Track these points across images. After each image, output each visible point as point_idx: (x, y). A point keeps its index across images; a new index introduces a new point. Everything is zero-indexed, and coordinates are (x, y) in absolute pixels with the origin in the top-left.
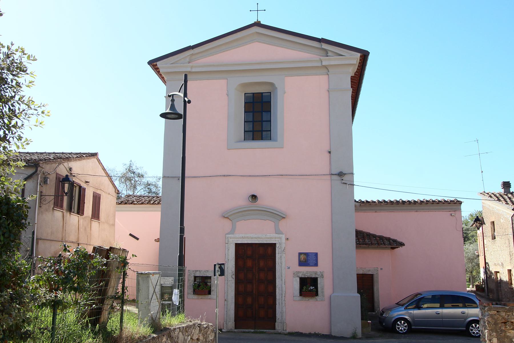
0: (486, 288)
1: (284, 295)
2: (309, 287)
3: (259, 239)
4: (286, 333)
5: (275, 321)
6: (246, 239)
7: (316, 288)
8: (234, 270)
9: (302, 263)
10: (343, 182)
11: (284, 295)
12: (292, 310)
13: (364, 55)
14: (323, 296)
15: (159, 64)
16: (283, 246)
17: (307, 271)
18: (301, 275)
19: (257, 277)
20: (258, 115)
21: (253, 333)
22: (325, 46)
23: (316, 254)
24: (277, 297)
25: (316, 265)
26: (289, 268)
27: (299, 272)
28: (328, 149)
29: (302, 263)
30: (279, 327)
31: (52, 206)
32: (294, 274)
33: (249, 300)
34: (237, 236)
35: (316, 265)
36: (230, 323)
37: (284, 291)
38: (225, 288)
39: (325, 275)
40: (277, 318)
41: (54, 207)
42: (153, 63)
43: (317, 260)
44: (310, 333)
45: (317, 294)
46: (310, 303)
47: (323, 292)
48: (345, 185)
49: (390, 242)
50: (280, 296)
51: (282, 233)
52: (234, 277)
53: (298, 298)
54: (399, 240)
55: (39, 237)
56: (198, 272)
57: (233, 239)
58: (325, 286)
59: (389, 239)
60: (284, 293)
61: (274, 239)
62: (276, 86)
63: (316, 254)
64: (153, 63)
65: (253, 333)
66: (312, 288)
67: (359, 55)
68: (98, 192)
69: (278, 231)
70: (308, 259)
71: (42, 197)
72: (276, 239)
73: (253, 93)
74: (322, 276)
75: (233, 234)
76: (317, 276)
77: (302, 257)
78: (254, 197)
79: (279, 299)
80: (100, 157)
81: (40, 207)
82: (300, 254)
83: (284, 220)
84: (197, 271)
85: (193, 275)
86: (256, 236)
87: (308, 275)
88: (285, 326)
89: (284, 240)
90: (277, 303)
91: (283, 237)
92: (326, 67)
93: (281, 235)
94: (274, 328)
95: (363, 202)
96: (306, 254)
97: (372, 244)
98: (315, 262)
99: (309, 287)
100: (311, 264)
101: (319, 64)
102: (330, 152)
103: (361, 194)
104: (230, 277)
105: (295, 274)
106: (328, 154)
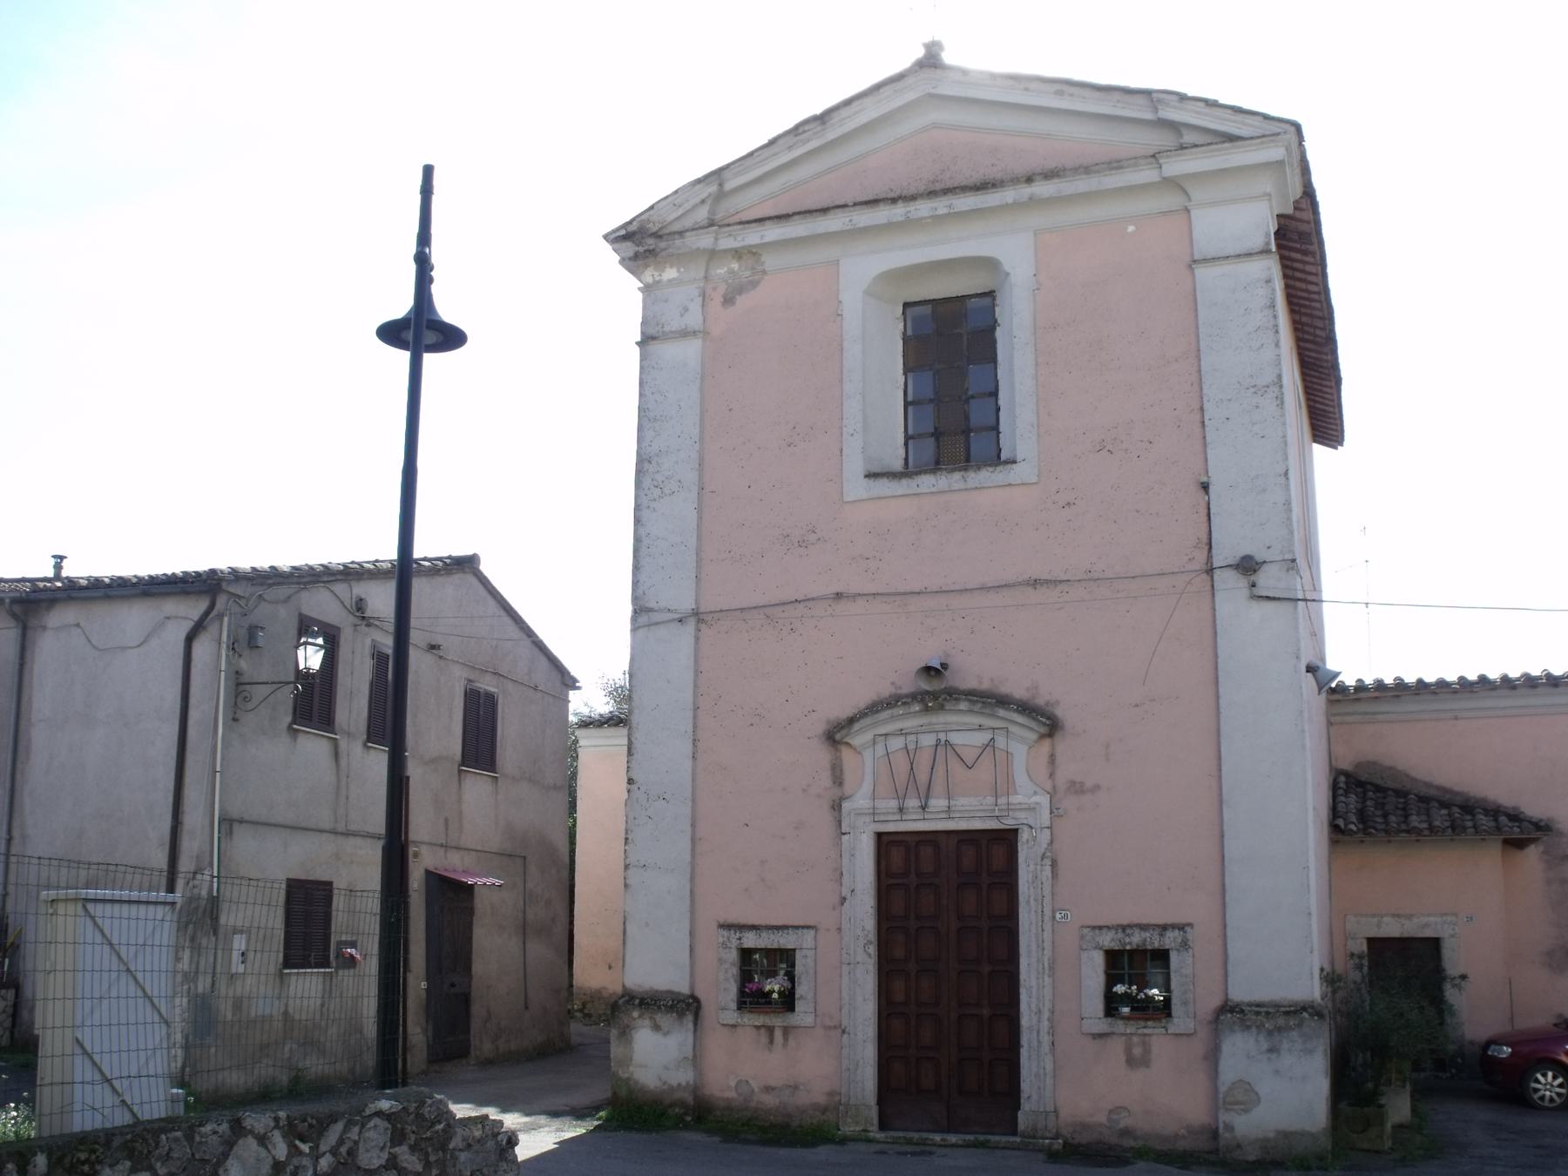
2: (1136, 975)
5: (1018, 1107)
8: (870, 923)
12: (1072, 1065)
24: (1025, 1021)
30: (1023, 1120)
31: (289, 719)
38: (845, 986)
40: (1024, 1096)
41: (294, 722)
49: (1496, 820)
50: (1035, 1018)
52: (872, 950)
54: (1534, 808)
55: (235, 814)
59: (1495, 812)
62: (1007, 267)
65: (968, 1145)
68: (487, 684)
71: (242, 688)
79: (1030, 1028)
80: (485, 568)
81: (235, 720)
90: (1024, 1040)
95: (1472, 684)
97: (1432, 830)
102: (421, 331)
104: (860, 950)
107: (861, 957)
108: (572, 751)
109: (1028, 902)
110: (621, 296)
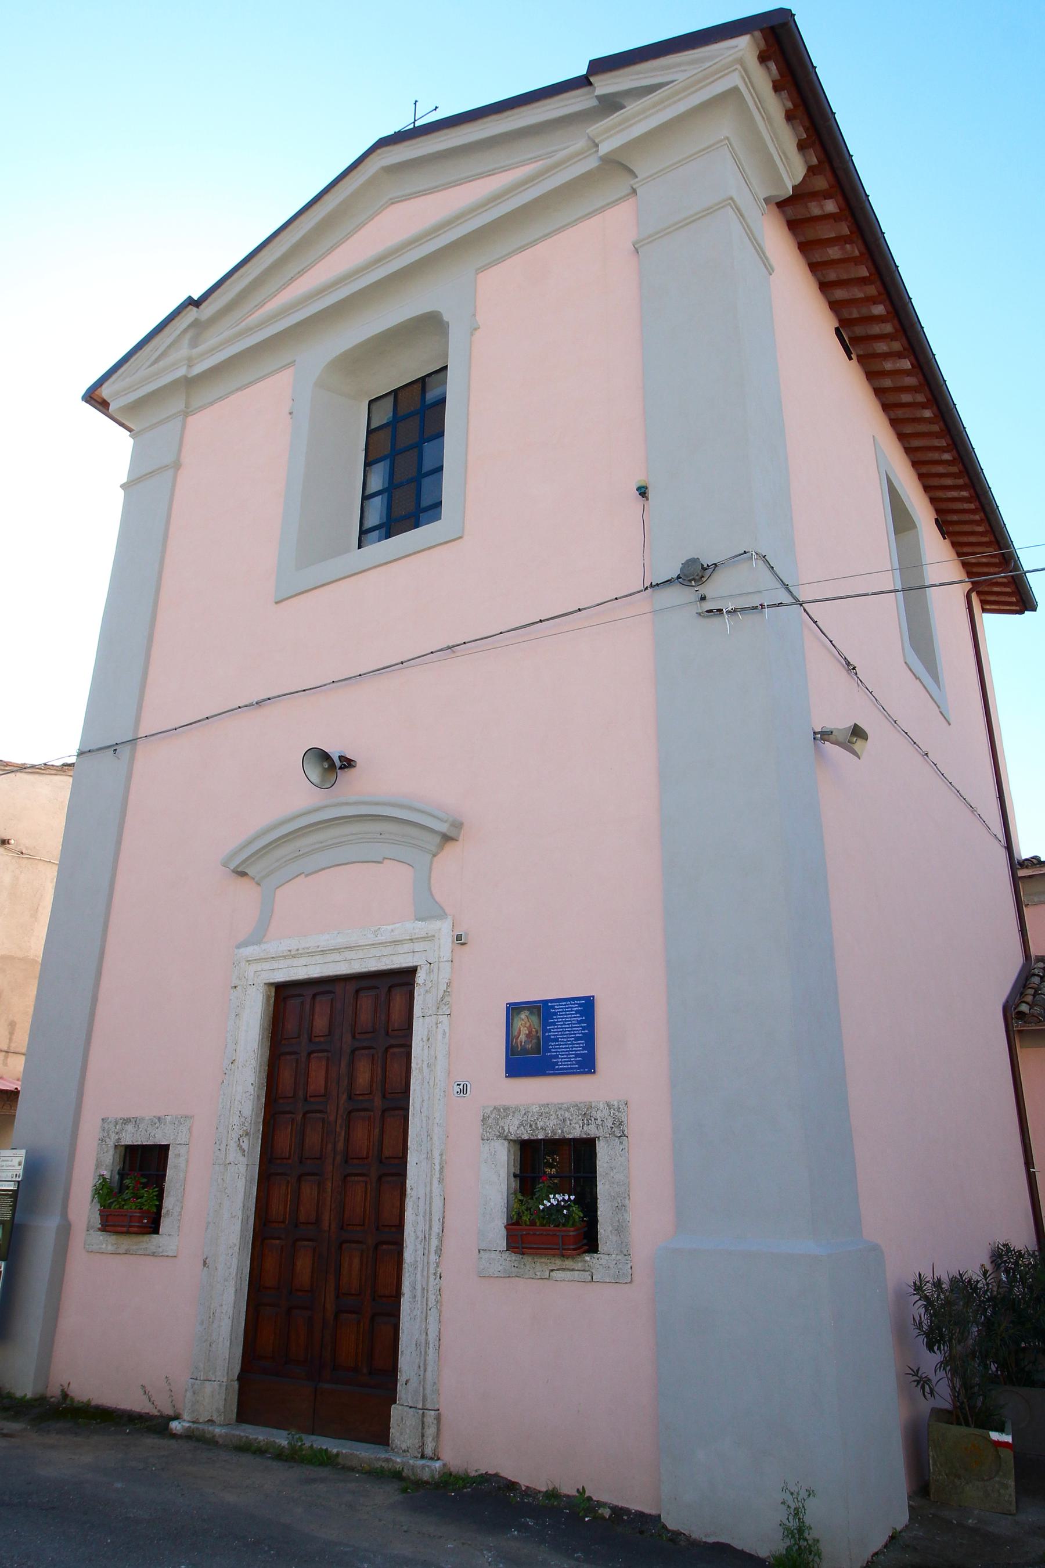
1: (434, 1242)
2: (557, 1196)
4: (426, 1476)
6: (303, 961)
7: (588, 1203)
9: (525, 1061)
10: (708, 605)
11: (434, 1242)
13: (778, 41)
14: (625, 1252)
15: (105, 392)
16: (445, 973)
17: (550, 1102)
18: (516, 1128)
19: (340, 1146)
21: (280, 1456)
22: (606, 85)
23: (587, 1006)
25: (587, 1065)
26: (463, 1091)
27: (505, 1111)
29: (525, 1061)
30: (402, 1422)
32: (484, 1119)
33: (304, 1265)
34: (272, 947)
35: (587, 1065)
36: (208, 1388)
37: (436, 1215)
39: (635, 1125)
42: (94, 397)
43: (589, 1039)
45: (589, 1242)
46: (558, 1290)
47: (620, 1229)
48: (716, 621)
51: (442, 915)
53: (502, 1261)
56: (130, 1127)
57: (258, 967)
58: (635, 1187)
60: (436, 1228)
61: (407, 947)
63: (587, 1006)
64: (94, 397)
65: (280, 1456)
67: (744, 45)
69: (429, 909)
70: (551, 1037)
72: (418, 946)
73: (395, 392)
75: (259, 942)
76: (592, 1131)
82: (514, 1009)
83: (450, 848)
84: (126, 1121)
86: (340, 941)
87: (548, 1128)
90: (406, 1288)
91: (444, 930)
92: (616, 165)
93: (433, 926)
94: (381, 1436)
96: (543, 1009)
98: (579, 1048)
99: (557, 1196)
100: (562, 1062)
104: (233, 1145)
105: (492, 1120)
107: (234, 1155)
108: (599, 98)
109: (421, 1070)
110: (121, 493)
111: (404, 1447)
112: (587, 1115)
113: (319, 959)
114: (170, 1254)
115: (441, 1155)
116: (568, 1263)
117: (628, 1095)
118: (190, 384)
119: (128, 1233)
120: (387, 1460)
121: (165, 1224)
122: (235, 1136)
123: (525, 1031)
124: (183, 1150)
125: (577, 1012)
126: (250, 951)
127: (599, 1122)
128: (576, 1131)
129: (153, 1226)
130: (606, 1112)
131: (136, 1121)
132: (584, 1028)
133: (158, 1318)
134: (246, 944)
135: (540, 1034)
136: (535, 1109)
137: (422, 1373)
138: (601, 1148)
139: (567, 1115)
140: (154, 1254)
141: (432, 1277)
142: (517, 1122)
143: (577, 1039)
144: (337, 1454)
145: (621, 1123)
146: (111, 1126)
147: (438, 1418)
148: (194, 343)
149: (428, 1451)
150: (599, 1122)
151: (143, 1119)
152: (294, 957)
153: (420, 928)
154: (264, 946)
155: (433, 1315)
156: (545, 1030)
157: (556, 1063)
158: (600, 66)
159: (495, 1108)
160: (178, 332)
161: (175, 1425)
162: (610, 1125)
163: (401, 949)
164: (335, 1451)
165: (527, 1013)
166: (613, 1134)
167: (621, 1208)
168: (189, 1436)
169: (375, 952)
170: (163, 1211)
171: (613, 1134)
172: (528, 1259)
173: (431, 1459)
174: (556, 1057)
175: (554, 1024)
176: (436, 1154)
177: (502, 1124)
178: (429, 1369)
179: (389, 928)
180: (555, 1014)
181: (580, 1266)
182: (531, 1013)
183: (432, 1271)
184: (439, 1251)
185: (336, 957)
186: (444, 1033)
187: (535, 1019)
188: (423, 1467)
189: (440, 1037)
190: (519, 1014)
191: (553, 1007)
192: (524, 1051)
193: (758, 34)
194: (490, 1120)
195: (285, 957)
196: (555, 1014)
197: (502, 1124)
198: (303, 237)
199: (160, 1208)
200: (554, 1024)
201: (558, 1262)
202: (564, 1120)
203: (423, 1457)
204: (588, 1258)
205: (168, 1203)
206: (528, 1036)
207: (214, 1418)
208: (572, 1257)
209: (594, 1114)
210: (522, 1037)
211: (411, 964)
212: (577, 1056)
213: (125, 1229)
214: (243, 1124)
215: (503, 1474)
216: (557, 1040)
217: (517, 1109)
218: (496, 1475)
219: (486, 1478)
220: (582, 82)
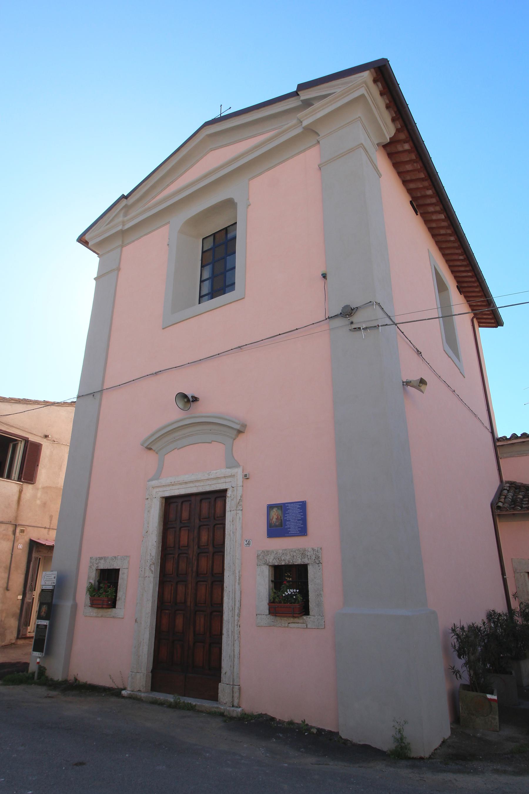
0: (207, 704)
1: (237, 611)
2: (290, 590)
3: (198, 484)
4: (234, 715)
6: (177, 487)
9: (276, 530)
10: (354, 326)
13: (382, 72)
18: (272, 560)
19: (195, 568)
20: (217, 264)
21: (171, 706)
23: (303, 506)
25: (303, 531)
26: (249, 544)
27: (267, 553)
28: (322, 270)
29: (276, 530)
33: (179, 621)
34: (164, 481)
36: (138, 676)
43: (304, 520)
44: (291, 723)
45: (305, 610)
46: (292, 634)
47: (319, 605)
53: (266, 619)
57: (158, 490)
58: (325, 586)
61: (223, 480)
63: (303, 506)
64: (82, 240)
65: (171, 706)
66: (289, 592)
67: (367, 75)
70: (287, 519)
73: (214, 235)
74: (318, 561)
76: (306, 561)
77: (275, 513)
78: (187, 400)
82: (270, 507)
83: (242, 437)
84: (101, 558)
85: (94, 568)
87: (286, 560)
88: (236, 695)
89: (240, 477)
91: (239, 472)
94: (215, 697)
96: (283, 507)
99: (290, 590)
101: (299, 130)
103: (503, 430)
104: (147, 568)
105: (261, 557)
106: (321, 282)
107: (148, 573)
109: (230, 535)
110: (94, 282)
111: (225, 702)
112: (303, 553)
113: (184, 486)
114: (121, 617)
115: (239, 572)
116: (296, 620)
117: (321, 544)
118: (123, 233)
119: (102, 608)
120: (217, 708)
121: (118, 604)
122: (148, 565)
123: (275, 517)
124: (126, 571)
125: (298, 508)
126: (154, 483)
127: (309, 557)
128: (299, 561)
129: (113, 604)
130: (312, 552)
131: (105, 559)
132: (302, 515)
133: (114, 645)
134: (151, 480)
135: (282, 518)
136: (280, 551)
137: (232, 669)
138: (310, 569)
139: (295, 554)
140: (114, 617)
141: (236, 626)
142: (272, 557)
143: (299, 520)
144: (195, 705)
145: (319, 557)
146: (94, 561)
147: (240, 689)
148: (125, 215)
149: (236, 704)
150: (309, 557)
151: (108, 557)
152: (173, 485)
153: (229, 472)
154: (160, 481)
155: (237, 643)
156: (284, 516)
157: (289, 531)
158: (302, 87)
159: (263, 551)
160: (118, 210)
161: (124, 692)
162: (314, 558)
163: (220, 481)
164: (194, 704)
165: (276, 509)
166: (315, 562)
167: (319, 595)
168: (130, 697)
169: (209, 482)
170: (118, 598)
171: (315, 562)
172: (278, 619)
173: (237, 707)
174: (289, 528)
175: (288, 513)
176: (237, 572)
177: (266, 558)
178: (235, 667)
179: (215, 472)
180: (289, 509)
181: (301, 621)
182: (278, 509)
183: (236, 624)
184: (239, 615)
185: (191, 485)
186: (240, 518)
187: (280, 512)
188: (233, 711)
189: (238, 520)
190: (273, 509)
191: (288, 506)
192: (276, 526)
193: (373, 70)
194: (261, 557)
195: (169, 485)
196: (289, 509)
197: (266, 558)
198: (173, 166)
199: (116, 596)
200: (288, 513)
201: (292, 620)
202: (293, 556)
203: (233, 706)
204: (305, 618)
205: (120, 594)
206: (277, 519)
207: (141, 689)
208: (298, 617)
209: (306, 553)
210: (274, 520)
211: (225, 488)
212: (299, 527)
213: (101, 606)
214: (152, 559)
215: (269, 714)
216: (290, 521)
217: (273, 552)
218: (266, 714)
219: (261, 715)
220: (295, 94)
